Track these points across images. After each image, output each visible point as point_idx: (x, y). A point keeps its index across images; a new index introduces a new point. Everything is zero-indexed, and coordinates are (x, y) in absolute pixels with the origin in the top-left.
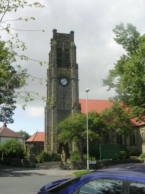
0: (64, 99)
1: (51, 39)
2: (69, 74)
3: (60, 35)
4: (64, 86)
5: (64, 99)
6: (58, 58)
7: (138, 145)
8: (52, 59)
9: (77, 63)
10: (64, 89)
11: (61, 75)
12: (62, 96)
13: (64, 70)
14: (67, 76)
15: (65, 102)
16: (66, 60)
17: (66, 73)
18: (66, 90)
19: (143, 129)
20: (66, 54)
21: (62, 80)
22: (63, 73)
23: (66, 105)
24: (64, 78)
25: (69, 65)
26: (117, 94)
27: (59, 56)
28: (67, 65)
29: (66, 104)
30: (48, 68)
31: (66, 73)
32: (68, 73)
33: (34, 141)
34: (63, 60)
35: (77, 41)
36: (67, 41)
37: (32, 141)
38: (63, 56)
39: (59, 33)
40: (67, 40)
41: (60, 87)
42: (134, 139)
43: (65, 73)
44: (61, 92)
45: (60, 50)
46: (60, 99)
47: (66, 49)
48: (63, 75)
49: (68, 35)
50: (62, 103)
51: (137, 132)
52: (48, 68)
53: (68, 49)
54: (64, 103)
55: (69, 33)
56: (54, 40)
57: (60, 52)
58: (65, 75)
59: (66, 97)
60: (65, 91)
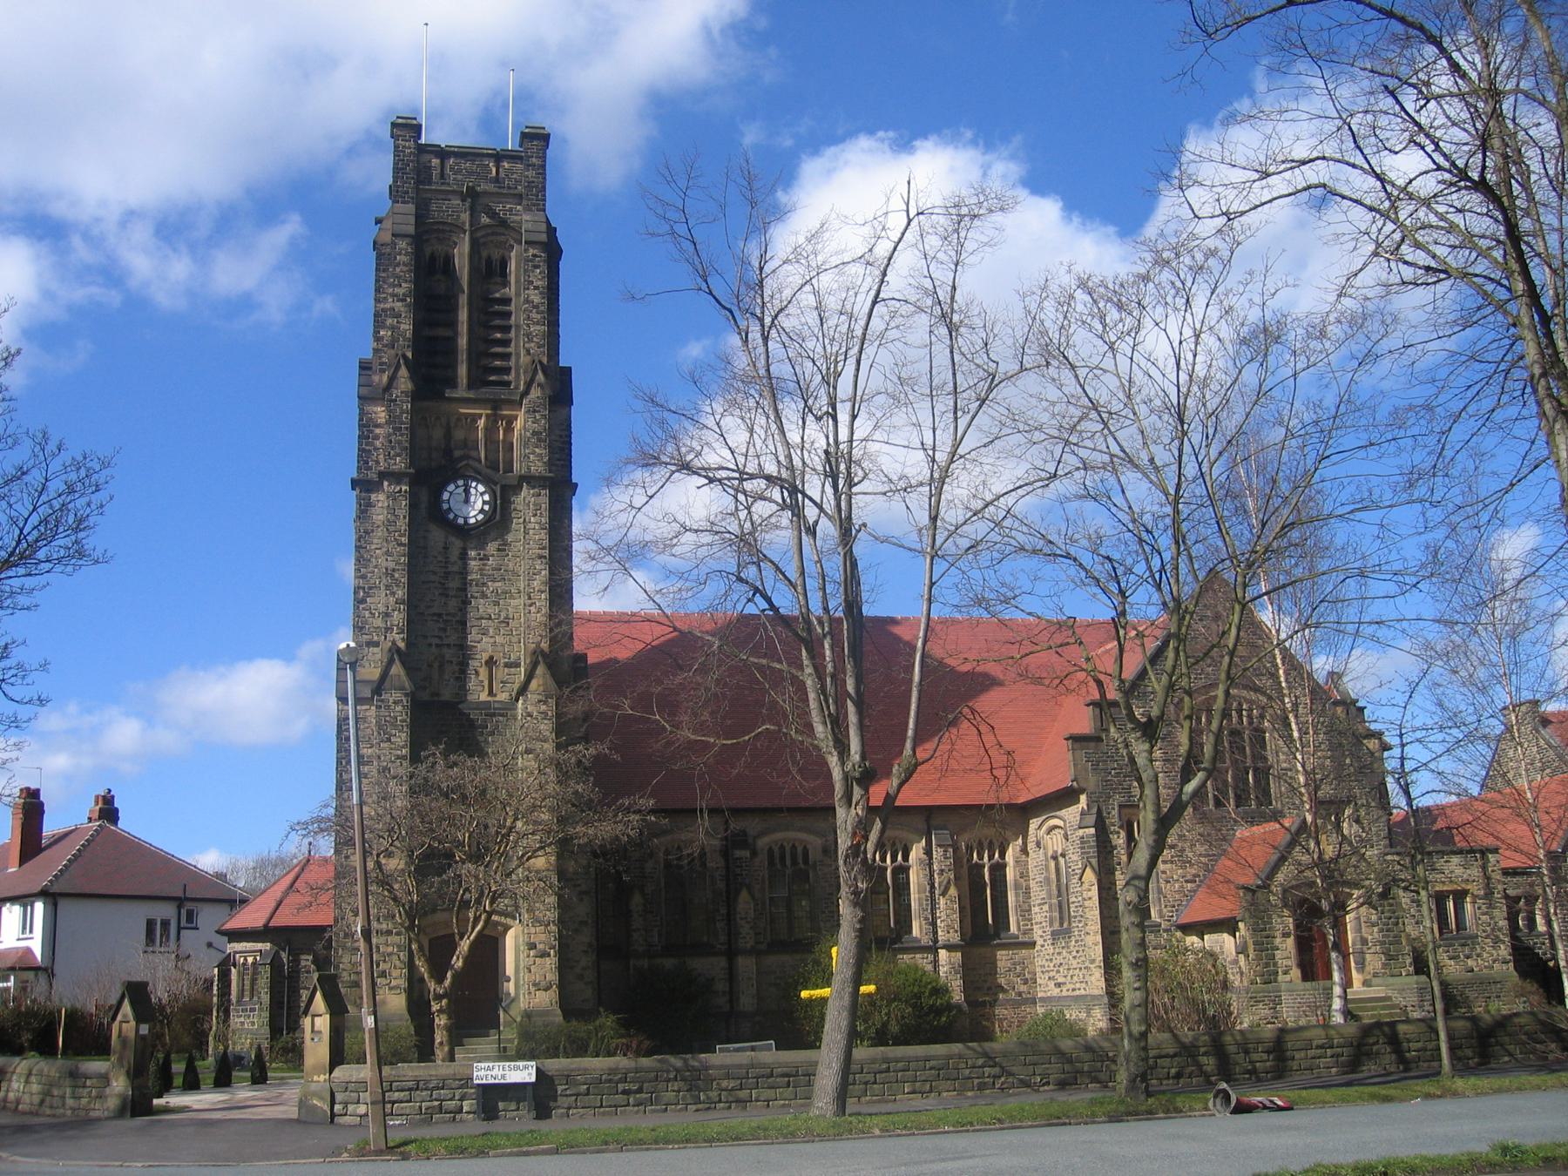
44: (447, 574)
50: (447, 657)
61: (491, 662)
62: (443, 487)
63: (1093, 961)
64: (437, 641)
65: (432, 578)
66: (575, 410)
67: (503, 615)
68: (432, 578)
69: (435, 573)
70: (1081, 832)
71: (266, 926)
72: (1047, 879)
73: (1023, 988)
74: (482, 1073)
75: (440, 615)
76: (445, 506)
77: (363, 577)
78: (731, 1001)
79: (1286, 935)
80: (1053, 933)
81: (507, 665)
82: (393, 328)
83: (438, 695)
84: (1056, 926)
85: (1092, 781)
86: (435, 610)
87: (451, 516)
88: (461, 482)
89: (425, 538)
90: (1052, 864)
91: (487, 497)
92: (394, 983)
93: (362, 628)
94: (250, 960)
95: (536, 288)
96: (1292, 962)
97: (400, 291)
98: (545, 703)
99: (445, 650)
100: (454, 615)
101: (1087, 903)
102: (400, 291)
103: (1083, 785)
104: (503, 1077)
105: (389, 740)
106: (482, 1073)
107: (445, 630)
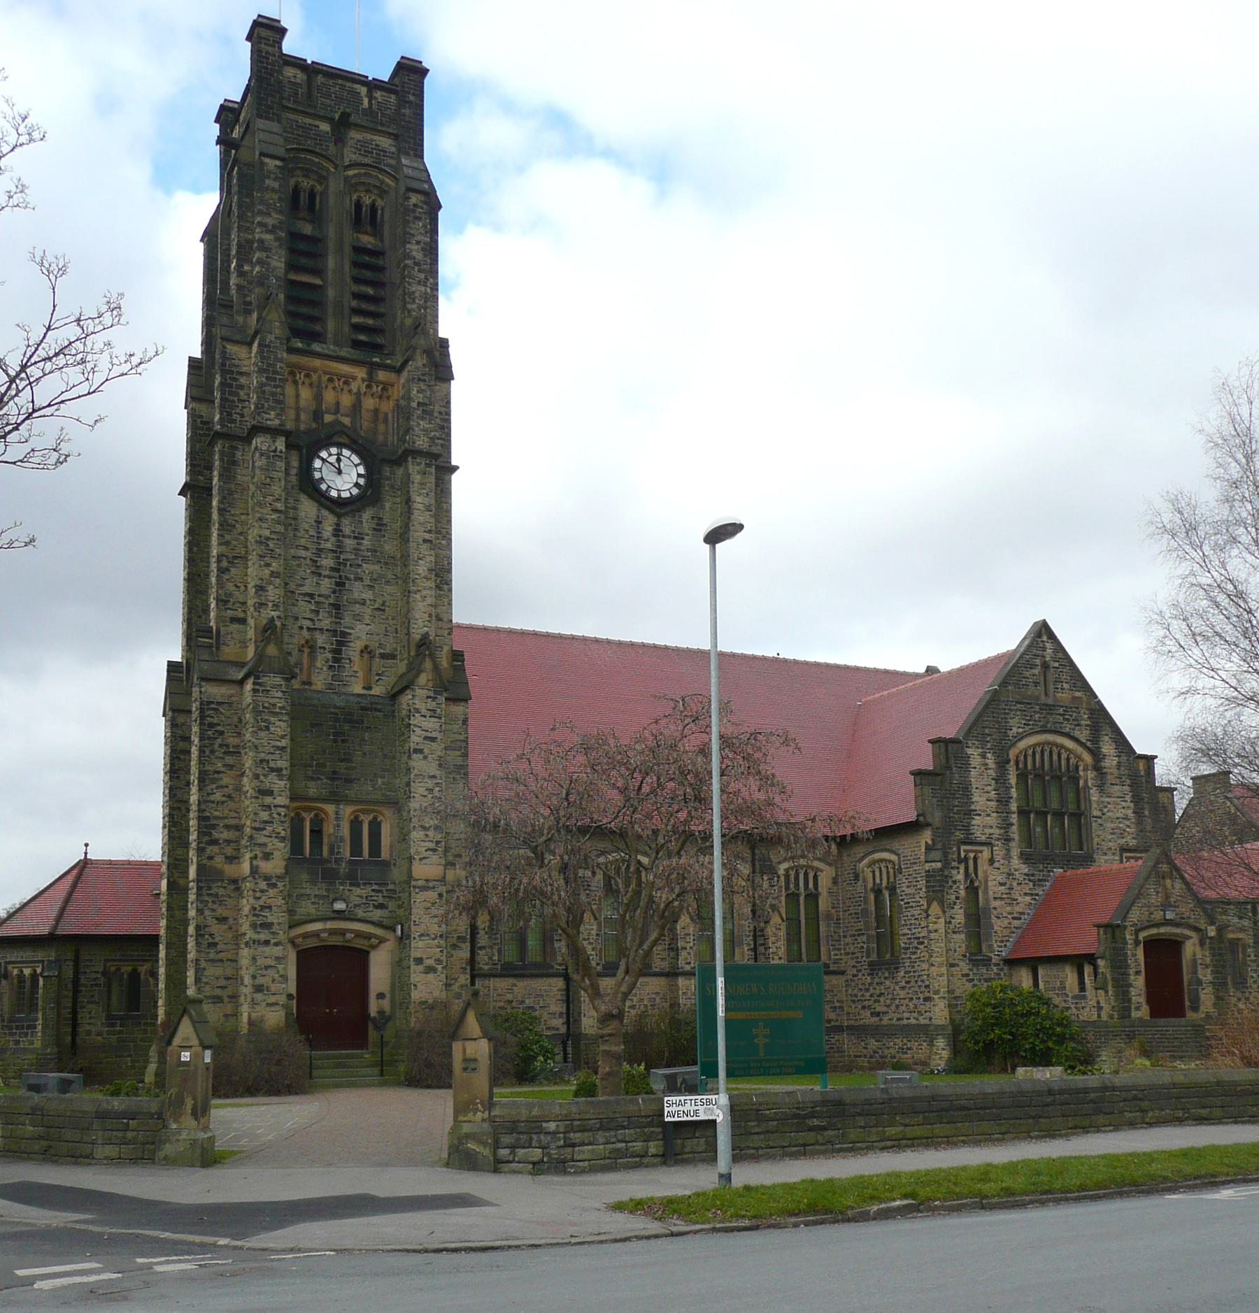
0: (336, 606)
1: (223, 108)
2: (376, 411)
3: (309, 81)
4: (339, 506)
5: (336, 606)
6: (292, 276)
7: (843, 973)
8: (241, 274)
9: (442, 334)
10: (337, 532)
11: (317, 415)
12: (326, 585)
13: (340, 377)
14: (365, 425)
15: (344, 634)
16: (356, 296)
17: (356, 408)
18: (359, 537)
19: (877, 856)
20: (358, 250)
21: (356, 460)
22: (329, 396)
23: (356, 657)
24: (344, 440)
25: (379, 340)
26: (1225, 512)
27: (303, 261)
28: (362, 338)
29: (358, 645)
30: (197, 354)
31: (356, 408)
32: (369, 403)
33: (59, 932)
34: (331, 293)
35: (448, 145)
36: (364, 143)
37: (44, 930)
38: (331, 262)
39: (299, 63)
40: (369, 136)
41: (308, 509)
42: (814, 918)
43: (346, 400)
44: (320, 551)
45: (311, 207)
46: (304, 608)
47: (296, 191)
48: (328, 418)
49: (378, 94)
50: (320, 642)
51: (835, 881)
52: (197, 354)
53: (373, 208)
54: (341, 639)
55: (383, 72)
56: (263, 111)
57: (307, 229)
58: (347, 421)
59: (356, 595)
60: (349, 543)
61: (366, 650)
62: (314, 454)
63: (937, 992)
64: (307, 623)
65: (303, 553)
66: (457, 389)
67: (379, 601)
68: (303, 553)
69: (306, 549)
70: (927, 866)
71: (50, 934)
72: (865, 912)
73: (833, 1016)
74: (674, 1108)
75: (311, 595)
76: (317, 475)
77: (227, 543)
78: (568, 1023)
79: (1138, 973)
80: (871, 964)
81: (383, 656)
82: (260, 262)
83: (310, 684)
84: (874, 957)
85: (936, 817)
86: (306, 589)
87: (324, 487)
88: (334, 450)
89: (295, 508)
90: (872, 897)
91: (361, 470)
92: (272, 999)
93: (226, 602)
94: (27, 972)
95: (418, 243)
96: (1142, 1000)
97: (270, 221)
98: (434, 699)
99: (317, 635)
100: (327, 597)
101: (932, 935)
102: (270, 221)
103: (930, 820)
104: (696, 1112)
105: (267, 728)
106: (674, 1108)
107: (317, 612)
